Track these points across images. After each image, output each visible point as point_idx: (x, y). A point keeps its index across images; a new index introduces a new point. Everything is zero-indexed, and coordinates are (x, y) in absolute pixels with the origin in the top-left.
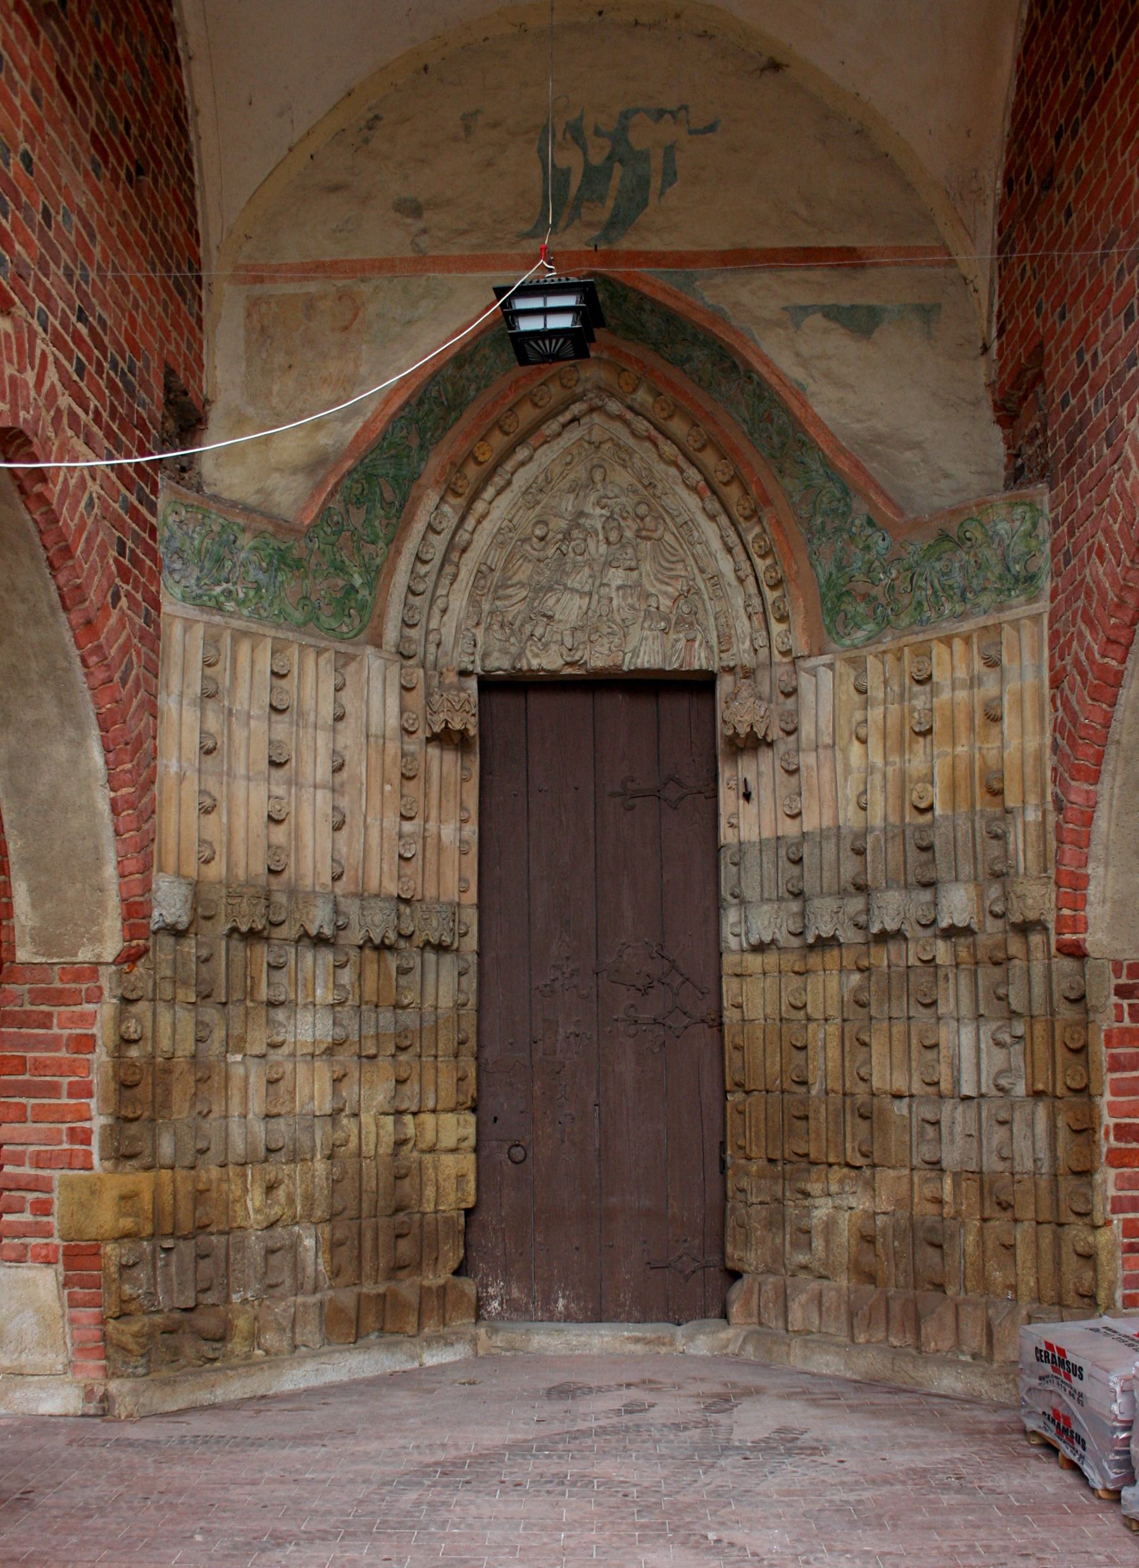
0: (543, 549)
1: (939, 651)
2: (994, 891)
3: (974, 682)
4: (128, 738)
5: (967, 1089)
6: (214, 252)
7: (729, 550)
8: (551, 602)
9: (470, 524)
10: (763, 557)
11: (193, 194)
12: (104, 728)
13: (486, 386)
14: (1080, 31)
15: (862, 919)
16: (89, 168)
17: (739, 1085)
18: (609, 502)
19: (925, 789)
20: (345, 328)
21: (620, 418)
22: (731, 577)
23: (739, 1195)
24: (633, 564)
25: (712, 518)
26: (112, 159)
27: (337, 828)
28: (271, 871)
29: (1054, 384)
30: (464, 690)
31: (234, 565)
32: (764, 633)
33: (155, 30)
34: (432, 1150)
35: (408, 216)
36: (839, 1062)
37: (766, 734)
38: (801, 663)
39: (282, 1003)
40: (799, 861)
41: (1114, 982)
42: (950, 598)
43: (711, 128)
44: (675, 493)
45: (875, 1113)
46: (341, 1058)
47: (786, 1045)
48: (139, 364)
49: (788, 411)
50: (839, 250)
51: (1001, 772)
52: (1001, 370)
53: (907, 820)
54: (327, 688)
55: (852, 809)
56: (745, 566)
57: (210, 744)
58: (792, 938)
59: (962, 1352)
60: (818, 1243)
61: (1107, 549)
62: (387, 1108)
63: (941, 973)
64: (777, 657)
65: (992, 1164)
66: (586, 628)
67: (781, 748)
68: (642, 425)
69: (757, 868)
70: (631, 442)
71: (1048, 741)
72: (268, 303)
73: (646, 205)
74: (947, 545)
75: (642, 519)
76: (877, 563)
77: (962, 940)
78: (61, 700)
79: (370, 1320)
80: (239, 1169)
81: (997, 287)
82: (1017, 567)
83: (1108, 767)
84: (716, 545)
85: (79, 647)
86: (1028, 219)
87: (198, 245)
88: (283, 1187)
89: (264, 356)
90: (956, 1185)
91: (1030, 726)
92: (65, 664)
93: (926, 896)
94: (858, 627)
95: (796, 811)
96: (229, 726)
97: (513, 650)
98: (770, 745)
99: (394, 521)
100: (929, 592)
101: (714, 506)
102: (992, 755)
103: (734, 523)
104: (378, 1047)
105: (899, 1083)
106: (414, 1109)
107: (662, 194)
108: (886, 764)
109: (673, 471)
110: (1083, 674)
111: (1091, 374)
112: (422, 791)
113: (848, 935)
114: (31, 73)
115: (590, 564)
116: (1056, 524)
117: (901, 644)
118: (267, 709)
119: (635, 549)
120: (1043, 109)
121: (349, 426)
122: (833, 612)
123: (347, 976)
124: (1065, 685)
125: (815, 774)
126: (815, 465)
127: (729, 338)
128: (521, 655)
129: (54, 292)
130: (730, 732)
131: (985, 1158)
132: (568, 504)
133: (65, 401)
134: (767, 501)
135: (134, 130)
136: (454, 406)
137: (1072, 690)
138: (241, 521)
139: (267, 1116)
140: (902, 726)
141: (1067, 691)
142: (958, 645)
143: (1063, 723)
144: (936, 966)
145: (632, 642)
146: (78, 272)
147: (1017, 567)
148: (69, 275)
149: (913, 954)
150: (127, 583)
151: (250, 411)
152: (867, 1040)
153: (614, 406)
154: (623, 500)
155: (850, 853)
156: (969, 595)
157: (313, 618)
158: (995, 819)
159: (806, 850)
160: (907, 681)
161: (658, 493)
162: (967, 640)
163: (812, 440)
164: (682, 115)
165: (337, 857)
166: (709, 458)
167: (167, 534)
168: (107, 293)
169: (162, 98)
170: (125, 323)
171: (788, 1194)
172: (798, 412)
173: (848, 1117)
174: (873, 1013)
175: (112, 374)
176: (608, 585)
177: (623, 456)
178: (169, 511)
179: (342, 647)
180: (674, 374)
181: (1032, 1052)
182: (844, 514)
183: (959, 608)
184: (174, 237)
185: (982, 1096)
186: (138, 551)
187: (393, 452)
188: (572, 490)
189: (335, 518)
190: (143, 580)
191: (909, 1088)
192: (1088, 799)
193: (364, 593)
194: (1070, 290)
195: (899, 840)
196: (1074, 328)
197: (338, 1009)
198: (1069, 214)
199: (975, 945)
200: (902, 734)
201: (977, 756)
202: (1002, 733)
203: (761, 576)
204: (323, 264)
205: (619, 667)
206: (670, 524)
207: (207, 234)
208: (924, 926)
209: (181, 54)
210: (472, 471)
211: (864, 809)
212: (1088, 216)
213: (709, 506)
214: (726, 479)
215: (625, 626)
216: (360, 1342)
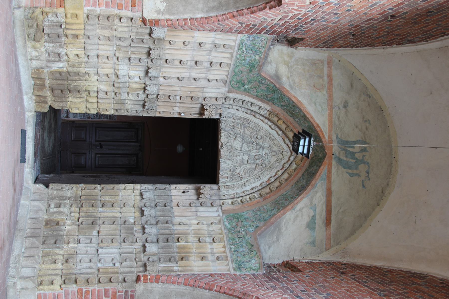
1: (222, 244)
2: (155, 258)
3: (213, 254)
4: (204, 24)
5: (100, 251)
6: (336, 52)
7: (252, 189)
8: (239, 140)
9: (262, 118)
10: (250, 198)
11: (350, 47)
12: (206, 18)
13: (298, 124)
14: (377, 280)
15: (149, 223)
16: (351, 24)
18: (266, 156)
19: (184, 240)
22: (245, 189)
23: (71, 188)
24: (249, 162)
25: (261, 184)
26: (354, 29)
27: (178, 78)
28: (167, 60)
29: (290, 275)
30: (216, 115)
31: (251, 54)
33: (389, 41)
36: (108, 216)
37: (201, 198)
38: (220, 208)
39: (130, 61)
41: (129, 290)
42: (236, 248)
43: (364, 186)
44: (268, 174)
48: (303, 32)
49: (288, 205)
50: (331, 220)
51: (188, 260)
52: (297, 263)
56: (247, 193)
57: (202, 45)
59: (25, 249)
61: (245, 286)
64: (222, 201)
65: (79, 257)
66: (232, 149)
67: (197, 202)
68: (287, 166)
70: (282, 163)
71: (195, 273)
72: (322, 65)
75: (261, 165)
76: (246, 228)
78: (214, 7)
79: (38, 82)
80: (83, 47)
81: (319, 261)
82: (243, 265)
83: (188, 288)
84: (253, 185)
85: (227, 14)
86: (334, 269)
87: (337, 48)
89: (308, 64)
90: (73, 248)
91: (200, 268)
92: (223, 9)
93: (155, 240)
94: (229, 223)
95: (179, 206)
96: (207, 50)
97: (227, 129)
98: (198, 199)
99: (262, 97)
100: (237, 242)
101: (264, 185)
103: (259, 190)
104: (117, 87)
105: (102, 232)
107: (347, 173)
108: (191, 230)
109: (274, 174)
110: (213, 281)
111: (291, 283)
114: (370, 13)
115: (250, 150)
116: (253, 275)
118: (211, 61)
120: (361, 272)
121: (288, 86)
122: (234, 217)
123: (137, 79)
124: (210, 277)
125: (189, 211)
126: (273, 212)
127: (308, 189)
128: (225, 131)
129: (318, 14)
130: (201, 188)
131: (81, 255)
132: (266, 145)
133: (291, 15)
134: (264, 200)
135: (363, 35)
136: (293, 115)
137: (209, 279)
138: (262, 56)
139: (98, 56)
141: (209, 278)
142: (223, 249)
143: (200, 276)
144: (135, 243)
145: (228, 162)
146: (324, 20)
147: (243, 265)
148: (323, 18)
150: (245, 26)
151: (293, 60)
152: (115, 224)
154: (267, 160)
157: (236, 74)
158: (175, 259)
160: (214, 236)
161: (268, 170)
163: (280, 212)
164: (367, 178)
166: (277, 184)
167: (259, 36)
168: (320, 26)
169: (373, 41)
170: (313, 30)
172: (288, 208)
173: (93, 218)
174: (122, 225)
175: (299, 26)
176: (243, 155)
177: (279, 161)
178: (265, 37)
179: (228, 82)
180: (300, 175)
182: (260, 220)
183: (233, 250)
184: (338, 42)
186: (254, 29)
187: (281, 98)
188: (270, 146)
189: (263, 81)
190: (246, 30)
191: (100, 235)
192: (179, 283)
193: (243, 88)
194: (314, 278)
196: (304, 279)
197: (128, 77)
198: (333, 278)
202: (199, 261)
203: (244, 197)
205: (221, 158)
206: (260, 173)
207: (340, 50)
208: (146, 240)
209: (385, 47)
210: (275, 119)
211: (179, 224)
212: (331, 282)
213: (264, 183)
214: (271, 188)
215: (232, 160)
216: (31, 79)
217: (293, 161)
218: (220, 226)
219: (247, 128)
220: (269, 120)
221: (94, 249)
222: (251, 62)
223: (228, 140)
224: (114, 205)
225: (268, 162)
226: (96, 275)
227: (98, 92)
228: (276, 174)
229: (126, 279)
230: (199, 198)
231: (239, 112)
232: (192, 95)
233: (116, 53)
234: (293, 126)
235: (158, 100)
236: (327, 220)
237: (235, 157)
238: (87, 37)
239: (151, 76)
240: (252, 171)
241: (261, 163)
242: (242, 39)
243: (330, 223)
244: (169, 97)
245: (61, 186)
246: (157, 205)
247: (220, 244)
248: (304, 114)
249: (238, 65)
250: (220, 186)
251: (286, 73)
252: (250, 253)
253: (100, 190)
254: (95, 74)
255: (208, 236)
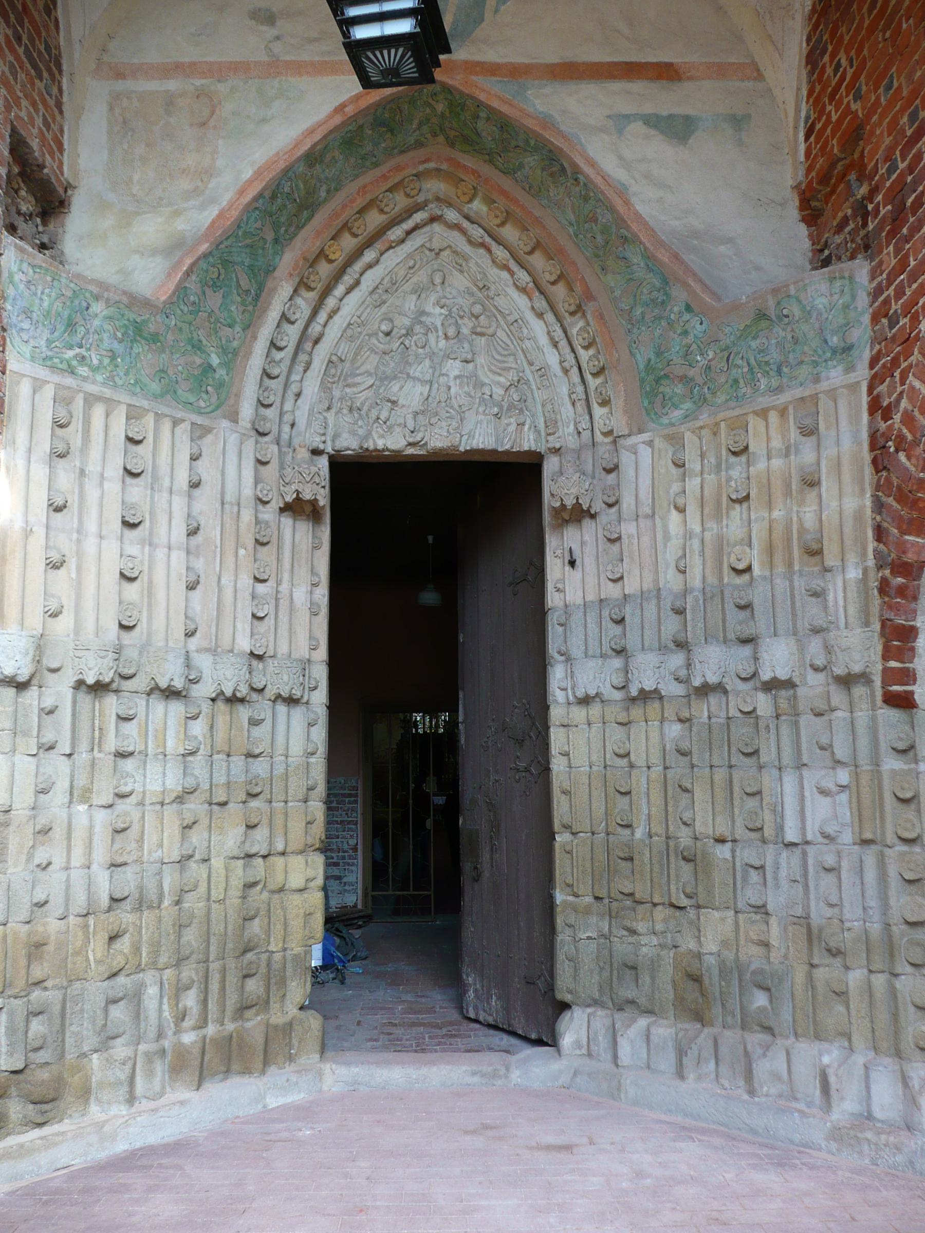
0: (389, 343)
1: (754, 423)
2: (815, 646)
5: (791, 835)
6: (77, 46)
7: (555, 345)
9: (322, 317)
10: (586, 348)
13: (337, 190)
15: (683, 673)
17: (567, 827)
18: (448, 302)
20: (203, 124)
21: (457, 227)
24: (469, 357)
25: (540, 315)
27: (191, 587)
28: (123, 627)
32: (587, 417)
34: (281, 890)
35: (262, 24)
37: (590, 506)
38: (621, 442)
40: (621, 621)
44: (506, 295)
45: (699, 857)
46: (192, 806)
47: (611, 790)
49: (612, 209)
50: (658, 65)
52: (809, 170)
53: (726, 580)
54: (184, 456)
55: (671, 573)
56: (570, 358)
58: (615, 691)
60: (645, 979)
62: (236, 853)
63: (762, 724)
64: (599, 438)
67: (603, 519)
68: (477, 232)
69: (581, 628)
70: (467, 249)
73: (483, 20)
74: (764, 324)
75: (477, 317)
76: (694, 346)
77: (783, 693)
84: (544, 340)
88: (127, 935)
93: (747, 650)
94: (675, 406)
95: (619, 575)
97: (361, 432)
99: (250, 308)
100: (746, 370)
101: (541, 304)
102: (809, 520)
103: (559, 318)
105: (723, 829)
106: (264, 852)
107: (496, 11)
108: (703, 530)
109: (505, 275)
112: (274, 557)
113: (672, 689)
115: (432, 355)
117: (718, 418)
118: (121, 471)
119: (471, 343)
121: (206, 213)
122: (652, 395)
123: (198, 728)
126: (636, 260)
127: (558, 142)
128: (368, 435)
130: (558, 504)
132: (411, 304)
134: (589, 296)
139: (113, 865)
140: (719, 494)
142: (773, 417)
145: (468, 427)
149: (734, 705)
152: (689, 786)
153: (452, 215)
154: (460, 300)
155: (670, 613)
156: (785, 370)
159: (628, 611)
160: (724, 452)
161: (491, 294)
162: (783, 412)
163: (636, 236)
165: (190, 614)
171: (615, 931)
172: (621, 209)
174: (695, 761)
176: (447, 375)
177: (460, 261)
179: (199, 420)
180: (506, 183)
181: (859, 801)
182: (663, 302)
183: (775, 383)
185: (807, 843)
187: (248, 241)
188: (414, 291)
189: (192, 298)
191: (733, 833)
195: (717, 599)
197: (190, 758)
199: (795, 697)
200: (719, 504)
201: (795, 519)
202: (820, 496)
203: (584, 366)
204: (183, 64)
205: (456, 448)
206: (502, 323)
210: (324, 270)
214: (553, 278)
217: (460, 211)
218: (688, 435)
219: (359, 364)
220: (326, 292)
221: (784, 854)
222: (119, 335)
223: (399, 425)
224: (622, 790)
225: (467, 296)
226: (888, 851)
227: (249, 856)
228: (506, 268)
229: (901, 746)
230: (593, 512)
231: (304, 392)
232: (250, 543)
233: (99, 804)
234: (344, 207)
235: (272, 654)
236: (659, 77)
237: (453, 400)
238: (39, 912)
239: (183, 680)
240: (499, 349)
241: (470, 319)
242: (28, 356)
243: (669, 65)
244: (261, 619)
245: (564, 961)
246: (619, 649)
247: (755, 428)
248: (299, 159)
249: (136, 382)
250: (549, 449)
251: (159, 220)
252: (786, 320)
253: (573, 834)
254: (182, 870)
255: (723, 473)
